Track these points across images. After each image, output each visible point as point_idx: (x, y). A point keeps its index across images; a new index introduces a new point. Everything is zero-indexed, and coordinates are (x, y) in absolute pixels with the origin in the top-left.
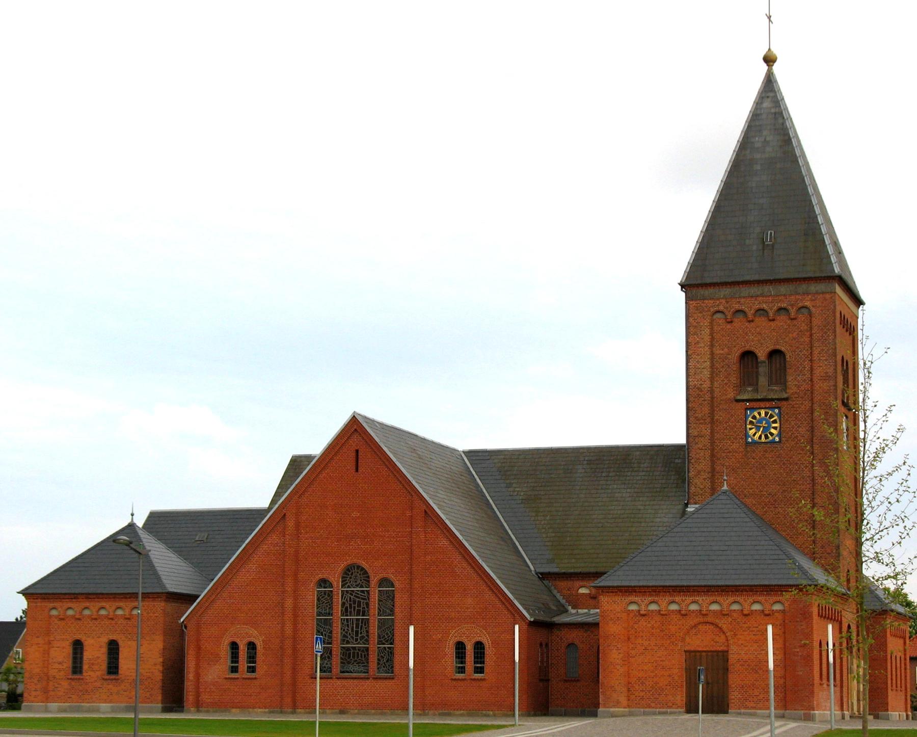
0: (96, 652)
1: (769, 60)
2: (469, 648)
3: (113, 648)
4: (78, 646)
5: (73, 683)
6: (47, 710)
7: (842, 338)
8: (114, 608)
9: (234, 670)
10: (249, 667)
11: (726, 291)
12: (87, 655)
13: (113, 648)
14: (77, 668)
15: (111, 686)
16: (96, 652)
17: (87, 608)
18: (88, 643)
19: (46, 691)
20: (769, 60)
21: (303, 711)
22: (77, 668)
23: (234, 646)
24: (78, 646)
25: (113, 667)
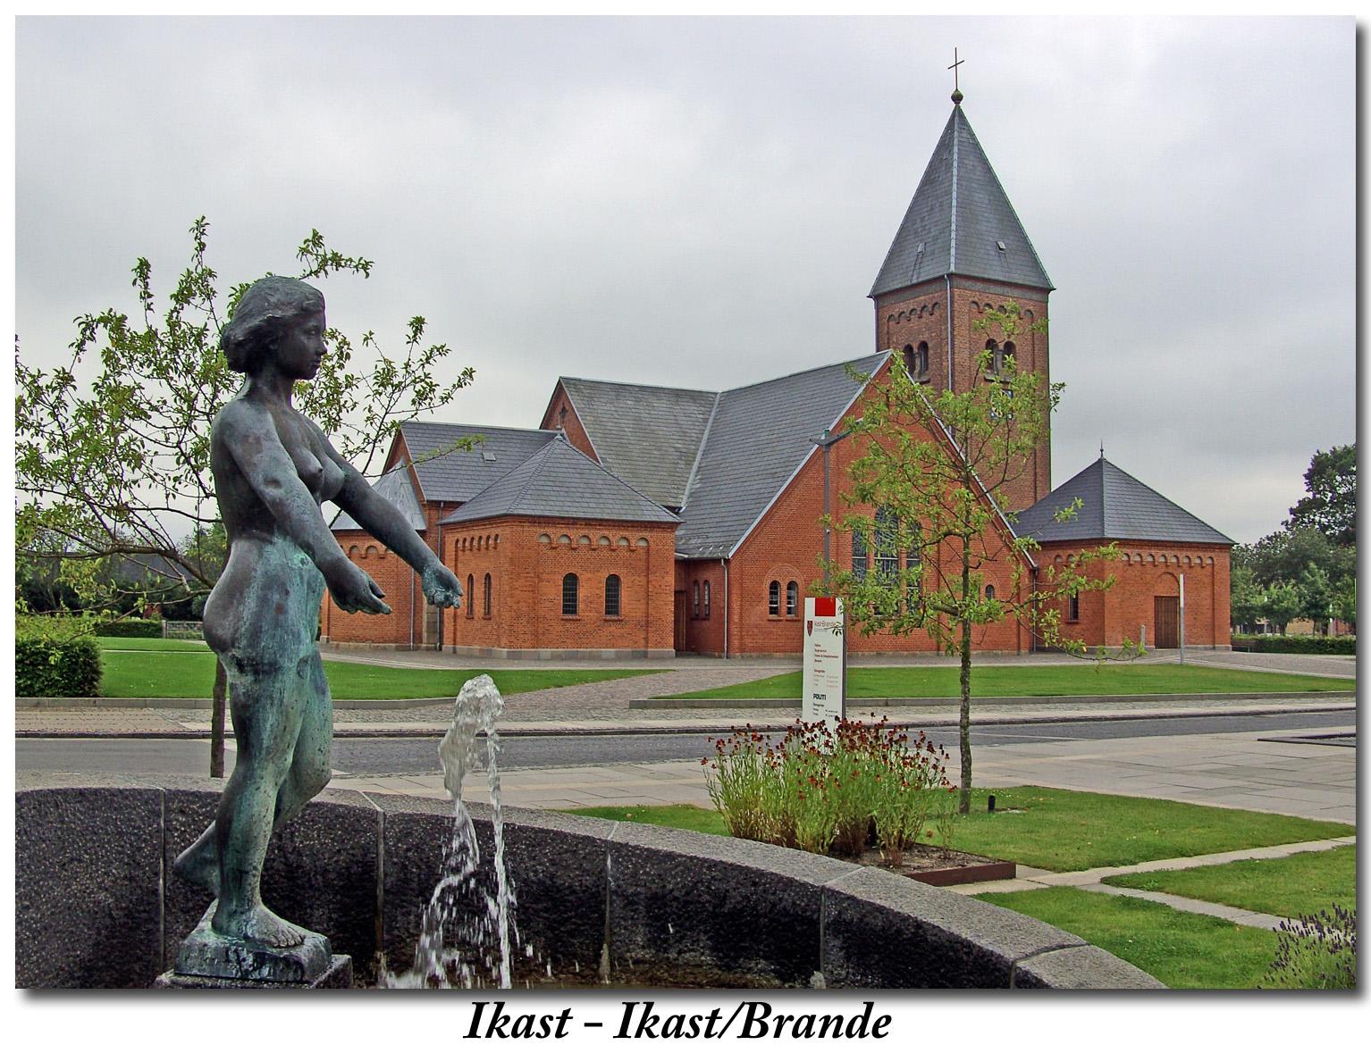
0: (591, 591)
1: (957, 98)
2: (784, 586)
3: (613, 583)
4: (571, 582)
5: (568, 625)
6: (538, 659)
7: (260, 283)
8: (559, 535)
9: (774, 611)
10: (771, 608)
11: (979, 286)
12: (582, 593)
13: (613, 583)
14: (570, 606)
15: (613, 628)
16: (591, 591)
17: (1058, 556)
18: (583, 577)
19: (536, 634)
20: (957, 98)
21: (782, 655)
22: (570, 606)
23: (774, 586)
24: (571, 582)
25: (612, 605)
